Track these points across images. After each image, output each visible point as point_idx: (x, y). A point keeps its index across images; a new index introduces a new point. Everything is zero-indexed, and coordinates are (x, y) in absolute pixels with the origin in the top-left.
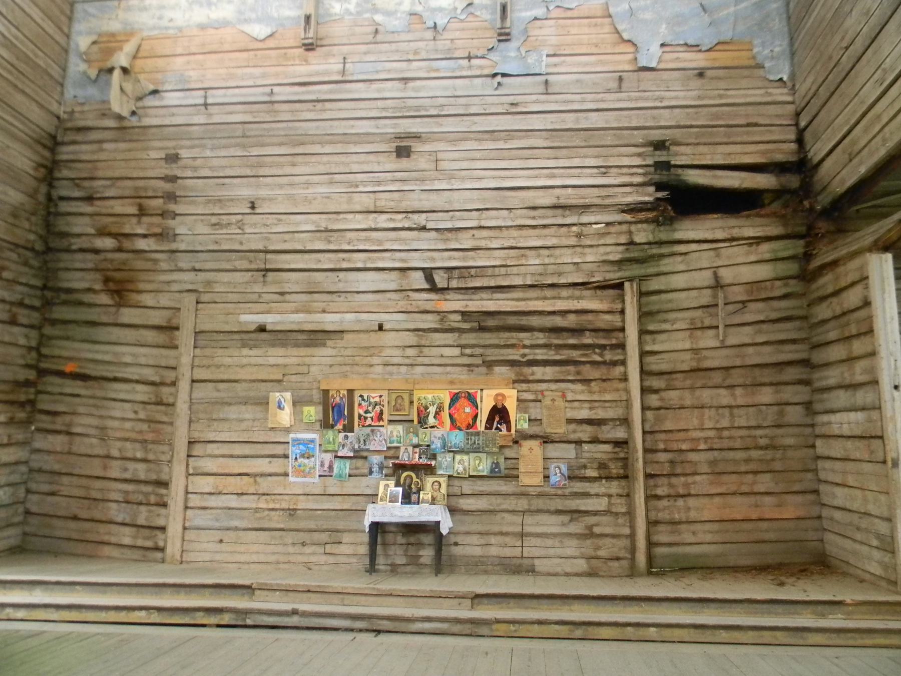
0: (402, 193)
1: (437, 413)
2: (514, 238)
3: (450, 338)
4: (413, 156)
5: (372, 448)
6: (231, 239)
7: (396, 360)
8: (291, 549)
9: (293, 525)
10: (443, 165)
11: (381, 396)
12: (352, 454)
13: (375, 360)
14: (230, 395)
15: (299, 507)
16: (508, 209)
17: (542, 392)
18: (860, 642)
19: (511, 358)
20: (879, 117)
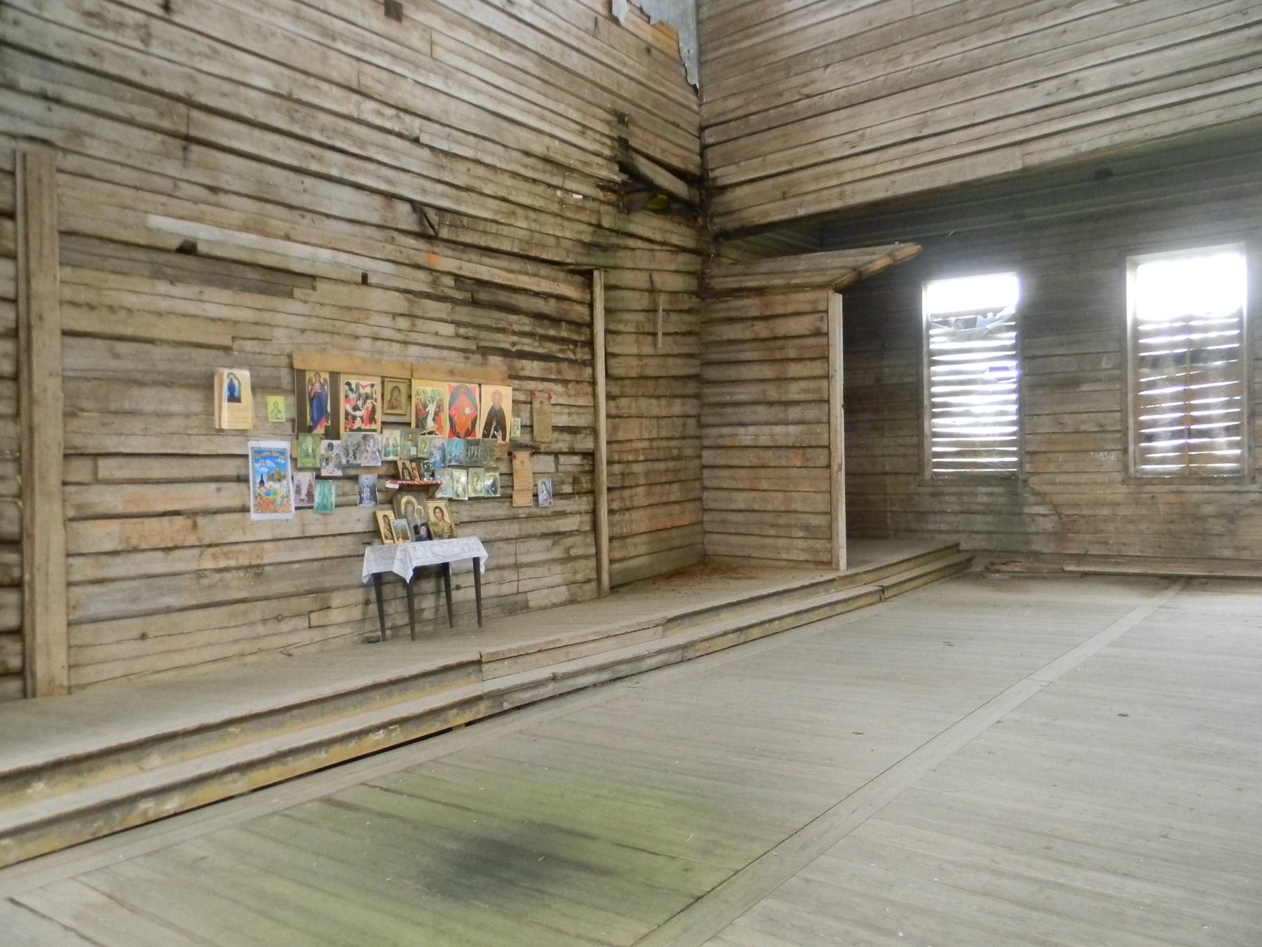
0: (392, 76)
1: (436, 414)
2: (507, 187)
3: (441, 309)
4: (405, 23)
5: (364, 463)
6: (125, 57)
7: (386, 333)
8: (261, 629)
9: (262, 590)
10: (439, 53)
11: (372, 386)
12: (339, 473)
13: (361, 330)
14: (140, 367)
15: (266, 561)
16: (504, 146)
17: (532, 393)
18: (856, 605)
19: (502, 345)
20: (839, 174)
